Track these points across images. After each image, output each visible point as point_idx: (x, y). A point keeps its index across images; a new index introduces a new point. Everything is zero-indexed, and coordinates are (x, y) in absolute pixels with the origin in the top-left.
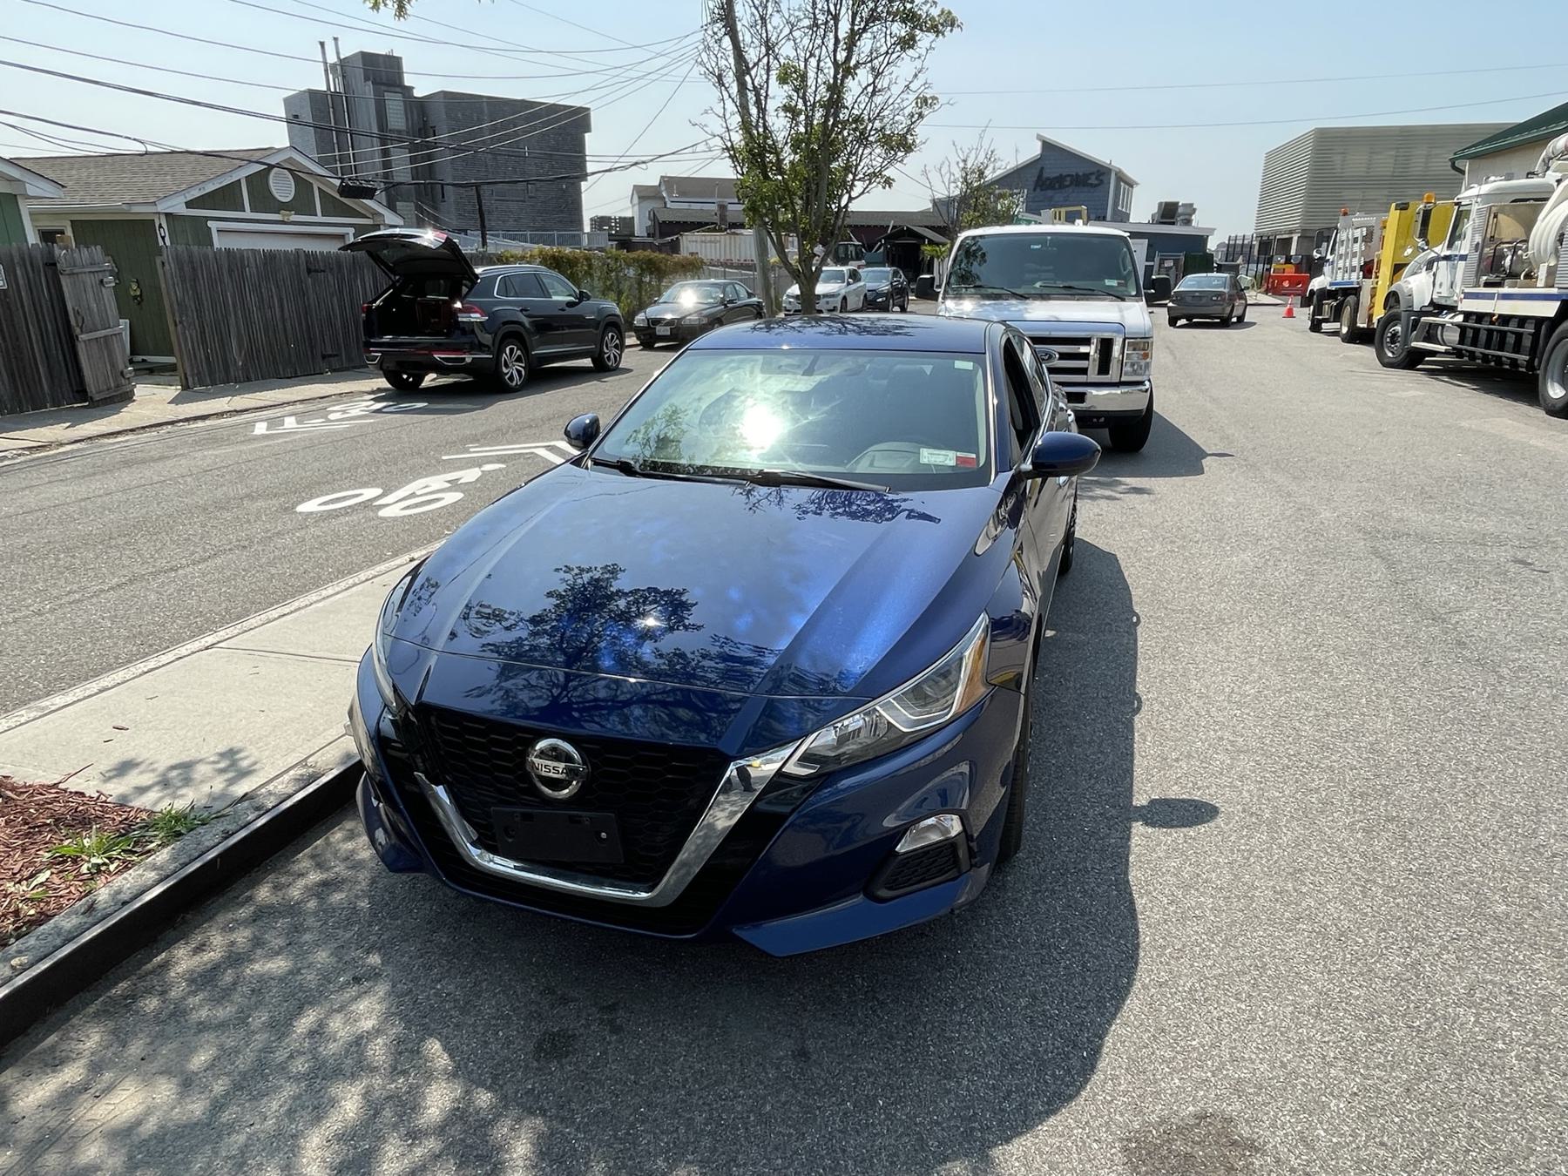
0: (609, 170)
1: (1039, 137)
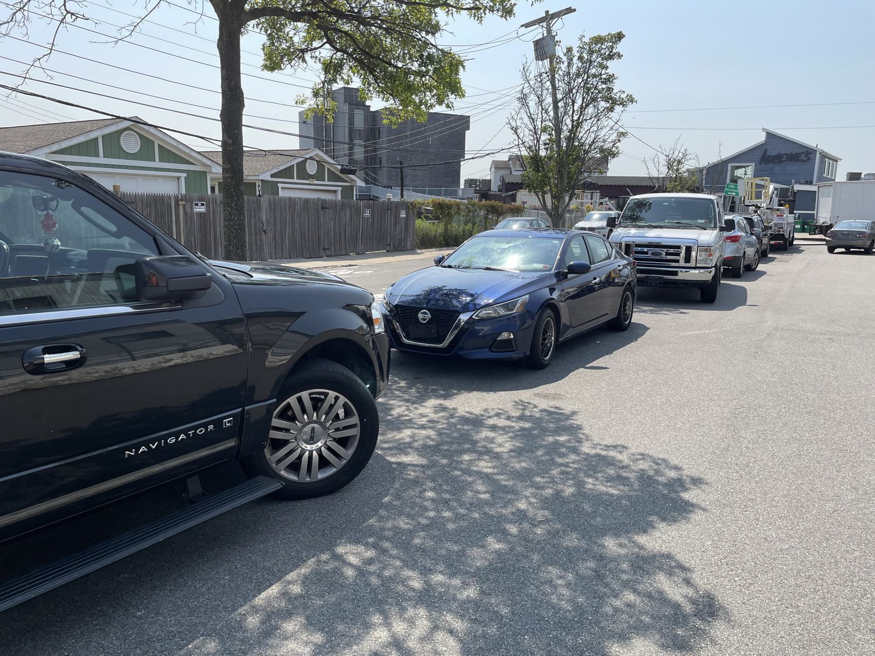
0: (473, 158)
1: (764, 129)
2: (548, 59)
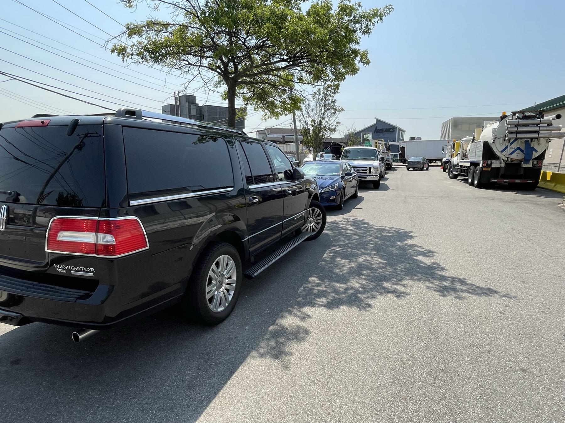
1: (375, 118)
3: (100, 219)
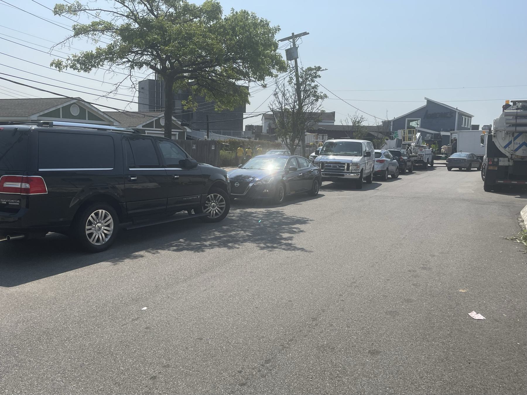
1: (426, 98)
2: (294, 60)
3: (24, 176)
